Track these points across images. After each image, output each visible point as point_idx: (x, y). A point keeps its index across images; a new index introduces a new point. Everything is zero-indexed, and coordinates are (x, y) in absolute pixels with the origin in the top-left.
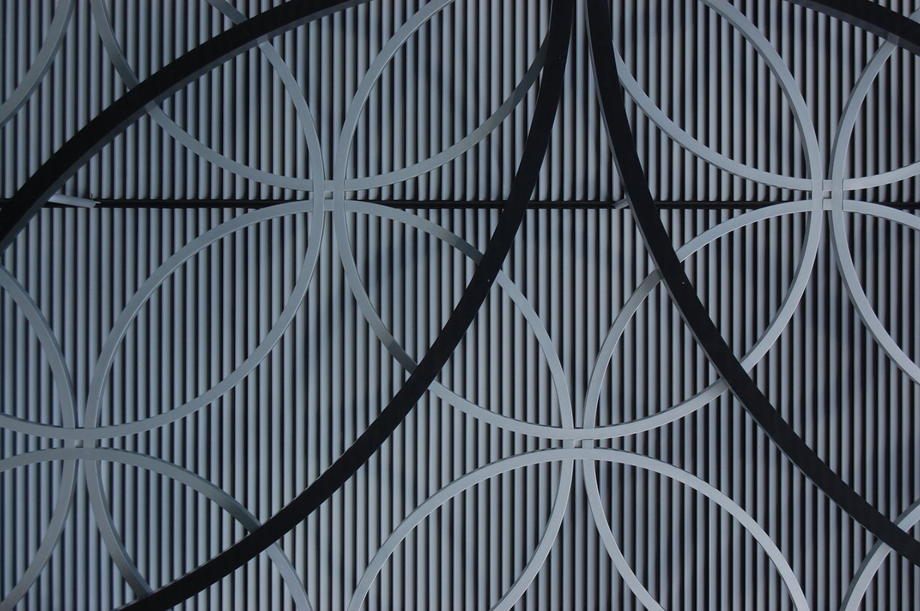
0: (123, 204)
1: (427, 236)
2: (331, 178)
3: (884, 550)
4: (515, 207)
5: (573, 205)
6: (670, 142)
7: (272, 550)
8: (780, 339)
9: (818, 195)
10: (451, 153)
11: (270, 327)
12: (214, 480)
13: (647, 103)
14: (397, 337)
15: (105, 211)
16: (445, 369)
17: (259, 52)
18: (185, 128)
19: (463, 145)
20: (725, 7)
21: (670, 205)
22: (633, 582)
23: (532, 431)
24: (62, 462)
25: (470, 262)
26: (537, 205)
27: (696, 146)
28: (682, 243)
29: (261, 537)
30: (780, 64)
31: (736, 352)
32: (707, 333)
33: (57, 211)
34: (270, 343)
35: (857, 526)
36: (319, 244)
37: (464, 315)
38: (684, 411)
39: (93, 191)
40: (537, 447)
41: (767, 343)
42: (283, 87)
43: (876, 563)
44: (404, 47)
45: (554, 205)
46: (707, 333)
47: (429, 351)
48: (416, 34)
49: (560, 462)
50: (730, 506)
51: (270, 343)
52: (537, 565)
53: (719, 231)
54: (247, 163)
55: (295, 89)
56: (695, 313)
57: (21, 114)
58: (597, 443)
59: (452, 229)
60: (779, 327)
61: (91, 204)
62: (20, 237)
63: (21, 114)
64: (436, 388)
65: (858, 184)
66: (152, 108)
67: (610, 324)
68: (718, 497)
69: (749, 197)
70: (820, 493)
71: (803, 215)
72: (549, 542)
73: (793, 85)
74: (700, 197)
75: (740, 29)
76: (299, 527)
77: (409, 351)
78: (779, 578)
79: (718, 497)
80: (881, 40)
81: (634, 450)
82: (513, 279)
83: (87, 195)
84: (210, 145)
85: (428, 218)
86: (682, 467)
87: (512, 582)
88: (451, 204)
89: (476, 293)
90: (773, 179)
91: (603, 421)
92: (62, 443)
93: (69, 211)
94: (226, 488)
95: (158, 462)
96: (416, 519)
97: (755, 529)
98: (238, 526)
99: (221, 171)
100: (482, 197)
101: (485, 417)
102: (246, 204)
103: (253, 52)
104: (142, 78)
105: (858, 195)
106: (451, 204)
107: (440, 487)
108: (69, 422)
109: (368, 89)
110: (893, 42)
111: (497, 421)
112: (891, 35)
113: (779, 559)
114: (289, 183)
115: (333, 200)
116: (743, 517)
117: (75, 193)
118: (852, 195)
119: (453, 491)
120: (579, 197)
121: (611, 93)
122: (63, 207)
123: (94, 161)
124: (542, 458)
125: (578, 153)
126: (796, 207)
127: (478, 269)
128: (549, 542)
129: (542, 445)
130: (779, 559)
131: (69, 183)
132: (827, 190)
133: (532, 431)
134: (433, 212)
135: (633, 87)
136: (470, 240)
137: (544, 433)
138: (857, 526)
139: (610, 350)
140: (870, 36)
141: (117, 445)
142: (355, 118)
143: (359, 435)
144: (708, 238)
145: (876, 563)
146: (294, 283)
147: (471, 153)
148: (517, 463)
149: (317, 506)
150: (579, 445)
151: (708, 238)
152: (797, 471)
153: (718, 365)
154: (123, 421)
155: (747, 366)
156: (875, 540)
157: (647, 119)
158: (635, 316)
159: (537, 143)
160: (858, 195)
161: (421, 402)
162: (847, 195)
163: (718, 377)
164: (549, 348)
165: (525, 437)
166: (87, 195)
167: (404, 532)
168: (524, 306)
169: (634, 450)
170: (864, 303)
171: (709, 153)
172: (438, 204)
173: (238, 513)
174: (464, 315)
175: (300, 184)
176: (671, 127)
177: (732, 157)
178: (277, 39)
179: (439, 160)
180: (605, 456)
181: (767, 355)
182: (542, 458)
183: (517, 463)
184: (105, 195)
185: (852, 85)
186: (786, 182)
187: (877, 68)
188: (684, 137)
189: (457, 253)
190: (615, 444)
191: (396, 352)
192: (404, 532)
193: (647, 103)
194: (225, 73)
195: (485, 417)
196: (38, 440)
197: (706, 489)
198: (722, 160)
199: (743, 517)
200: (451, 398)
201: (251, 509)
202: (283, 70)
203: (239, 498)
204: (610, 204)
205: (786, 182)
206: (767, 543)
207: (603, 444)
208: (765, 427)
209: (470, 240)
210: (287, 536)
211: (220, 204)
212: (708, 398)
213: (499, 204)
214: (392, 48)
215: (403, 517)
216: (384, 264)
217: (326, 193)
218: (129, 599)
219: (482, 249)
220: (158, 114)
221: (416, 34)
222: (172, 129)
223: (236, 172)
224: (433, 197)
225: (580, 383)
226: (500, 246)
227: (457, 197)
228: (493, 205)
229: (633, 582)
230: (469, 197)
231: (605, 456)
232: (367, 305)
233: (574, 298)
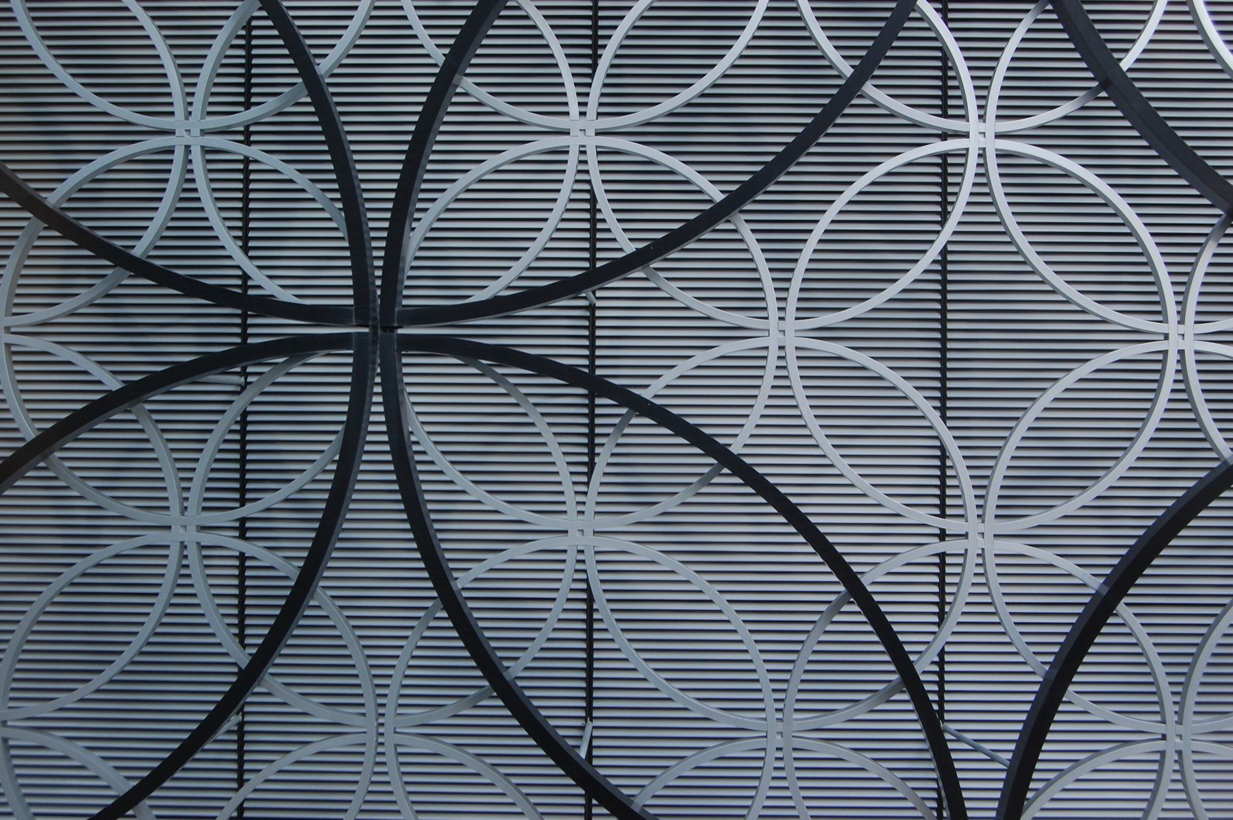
0: (589, 699)
1: (613, 455)
2: (566, 532)
3: (868, 88)
5: (592, 337)
6: (538, 259)
7: (865, 580)
8: (699, 172)
10: (548, 435)
11: (688, 582)
12: (809, 627)
13: (507, 278)
15: (595, 714)
16: (721, 441)
17: (464, 589)
18: (525, 649)
19: (541, 425)
20: (1223, 627)
22: (892, 291)
23: (770, 372)
24: (794, 749)
25: (634, 421)
26: (592, 367)
27: (542, 238)
28: (621, 250)
30: (476, 171)
31: (707, 207)
32: (690, 230)
33: (595, 752)
34: (700, 582)
35: (847, 111)
36: (623, 542)
37: (678, 426)
38: (756, 249)
39: (579, 723)
40: (785, 367)
41: (703, 182)
42: (492, 570)
43: (881, 96)
44: (463, 472)
45: (593, 352)
46: (690, 230)
47: (708, 454)
48: (453, 463)
49: (797, 348)
50: (832, 212)
51: (700, 582)
52: (881, 368)
54: (554, 600)
56: (675, 240)
58: (781, 319)
59: (608, 435)
60: (690, 172)
61: (590, 725)
62: (614, 782)
64: (736, 448)
65: (574, 109)
66: (508, 676)
67: (687, 308)
68: (825, 222)
69: (587, 206)
70: (847, 111)
71: (598, 153)
72: (863, 358)
73: (492, 161)
74: (587, 235)
75: (448, 203)
76: (840, 549)
77: (706, 470)
78: (889, 174)
79: (825, 222)
80: (459, 90)
81: (787, 290)
82: (647, 386)
83: (582, 728)
84: (540, 629)
85: (603, 445)
86: (801, 251)
87: (894, 388)
88: (591, 435)
89: (661, 415)
90: (569, 177)
91: (763, 314)
92: (779, 749)
93: (595, 743)
94: (815, 618)
95: (794, 672)
96: (843, 465)
97: (850, 193)
98: (846, 608)
99: (560, 620)
100: (586, 411)
101: (759, 409)
103: (465, 594)
104: (486, 683)
105: (583, 109)
106: (591, 435)
107: (817, 446)
108: (761, 743)
109: (496, 502)
110: (460, 80)
111: (763, 400)
112: (454, 82)
113: (874, 174)
115: (584, 529)
116: (840, 202)
117: (580, 737)
118: (583, 114)
119: (820, 435)
120: (586, 333)
121: (498, 306)
122: (591, 747)
123: (552, 722)
124: (793, 364)
125: (549, 332)
126: (592, 157)
127: (642, 414)
128: (863, 358)
129: (782, 363)
130: (874, 174)
131: (571, 742)
132: (579, 133)
133: (770, 372)
134: (597, 441)
136: (616, 421)
137: (772, 362)
138: (847, 111)
139: (709, 308)
140: (455, 99)
141: (780, 706)
142: (521, 512)
143: (775, 511)
144: (617, 229)
145: (881, 96)
146: (653, 562)
147: (548, 416)
148: (797, 384)
151: (617, 229)
152: (198, 756)
153: (716, 221)
154: (762, 700)
155: (719, 197)
156: (861, 96)
157: (521, 278)
158: (681, 289)
159: (543, 366)
160: (583, 109)
161: (748, 461)
162: (583, 118)
163: (728, 221)
164: (702, 357)
165: (776, 377)
166: (582, 728)
167: (853, 475)
168: (669, 377)
169: (787, 290)
170: (668, 105)
171: (548, 228)
172: (591, 446)
173: (836, 608)
174: (678, 426)
175: (571, 557)
176: (527, 258)
177: (551, 210)
178: (455, 575)
179: (553, 445)
180: (791, 313)
181: (712, 182)
182: (793, 364)
183: (797, 384)
184: (583, 714)
185: (496, 113)
186: (571, 167)
187: (482, 94)
188: (535, 248)
189: (627, 430)
190: (782, 305)
191: (706, 480)
192: (853, 475)
193: (507, 278)
194: (482, 616)
195: (759, 409)
196: (777, 759)
197: (818, 232)
198: (553, 218)
199: (840, 202)
200: (744, 436)
202: (478, 570)
203: (823, 608)
205: (571, 167)
206: (861, 183)
207: (782, 314)
208: (799, 155)
209: (616, 421)
210: (855, 569)
212: (746, 230)
213: (591, 396)
214: (464, 482)
215: (841, 475)
216: (634, 490)
217: (578, 535)
219: (624, 411)
221: (453, 463)
222: (526, 659)
223: (560, 611)
224: (585, 450)
225: (735, 332)
226: (624, 397)
227: (586, 430)
228: (592, 401)
229: (892, 291)
230: (586, 421)
231: (791, 313)
232: (667, 504)
233: (664, 335)
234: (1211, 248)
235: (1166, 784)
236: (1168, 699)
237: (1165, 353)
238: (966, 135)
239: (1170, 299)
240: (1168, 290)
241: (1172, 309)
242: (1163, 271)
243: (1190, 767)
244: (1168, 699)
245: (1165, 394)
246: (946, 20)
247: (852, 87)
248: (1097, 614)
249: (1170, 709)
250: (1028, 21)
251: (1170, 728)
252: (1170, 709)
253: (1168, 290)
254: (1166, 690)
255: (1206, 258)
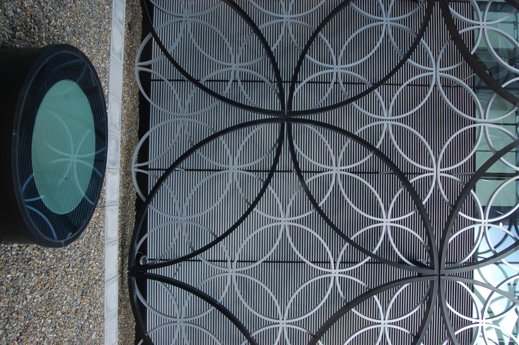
4: (272, 171)
7: (221, 242)
9: (333, 273)
14: (246, 198)
21: (303, 172)
23: (274, 218)
29: (218, 240)
31: (317, 202)
32: (311, 198)
37: (260, 195)
39: (184, 167)
43: (345, 247)
46: (311, 198)
53: (314, 178)
55: (226, 146)
57: (167, 154)
61: (184, 170)
62: (169, 177)
63: (167, 154)
64: (255, 209)
65: (342, 168)
66: (197, 150)
76: (228, 236)
77: (249, 201)
79: (313, 232)
83: (183, 168)
89: (263, 191)
96: (250, 237)
97: (320, 239)
101: (265, 215)
102: (216, 170)
106: (258, 171)
111: (267, 216)
113: (325, 245)
114: (225, 166)
115: (234, 169)
123: (184, 162)
126: (330, 173)
131: (179, 166)
133: (274, 218)
135: (296, 146)
145: (345, 247)
148: (271, 225)
149: (234, 229)
150: (285, 221)
157: (299, 154)
164: (278, 200)
166: (183, 168)
167: (247, 239)
170: (343, 191)
171: (312, 161)
172: (255, 171)
173: (213, 234)
174: (260, 195)
175: (227, 166)
183: (271, 225)
191: (246, 201)
192: (247, 239)
193: (299, 150)
194: (212, 143)
195: (265, 215)
198: (314, 162)
201: (216, 233)
202: (224, 142)
203: (213, 231)
204: (291, 171)
206: (323, 241)
211: (210, 170)
218: (190, 252)
220: (198, 151)
234: (305, 331)
235: (168, 318)
236: (189, 319)
237: (279, 319)
238: (335, 269)
239: (292, 321)
240: (294, 320)
241: (290, 321)
242: (299, 319)
243: (172, 325)
244: (189, 319)
245: (268, 319)
246: (367, 263)
247: (347, 240)
248: (212, 302)
249: (187, 320)
250: (364, 284)
251: (183, 320)
252: (187, 320)
253: (294, 320)
254: (192, 319)
255: (303, 330)
